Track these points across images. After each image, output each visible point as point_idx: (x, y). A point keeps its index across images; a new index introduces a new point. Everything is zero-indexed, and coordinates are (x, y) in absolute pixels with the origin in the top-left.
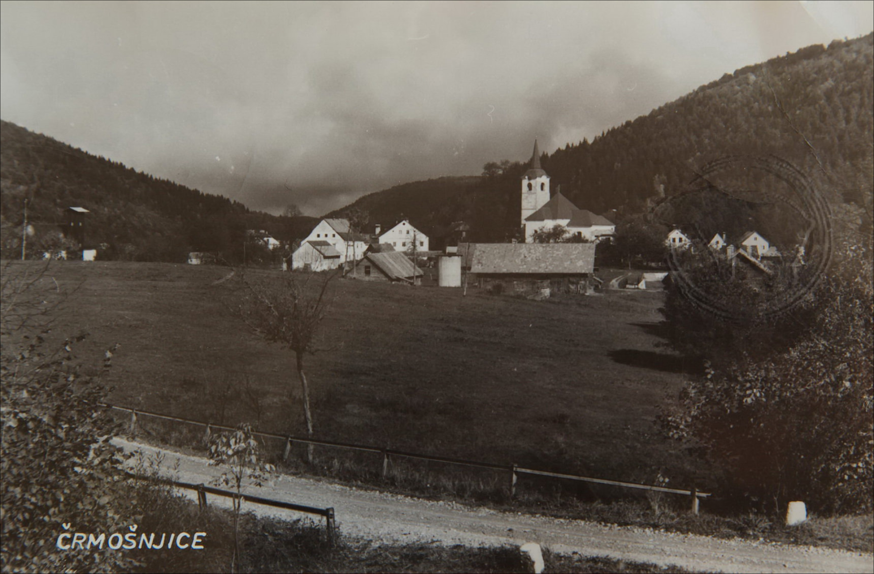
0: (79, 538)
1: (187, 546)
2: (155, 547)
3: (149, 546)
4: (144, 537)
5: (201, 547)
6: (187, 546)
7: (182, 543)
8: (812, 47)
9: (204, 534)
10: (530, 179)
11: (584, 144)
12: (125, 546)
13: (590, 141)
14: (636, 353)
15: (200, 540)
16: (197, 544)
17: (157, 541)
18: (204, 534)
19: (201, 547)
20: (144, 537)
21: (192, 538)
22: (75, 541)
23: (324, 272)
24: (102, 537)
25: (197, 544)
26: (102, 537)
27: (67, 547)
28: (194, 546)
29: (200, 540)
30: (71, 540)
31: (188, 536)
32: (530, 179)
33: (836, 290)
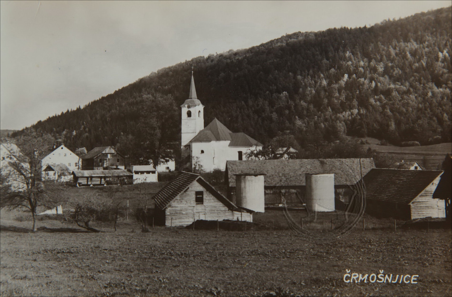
0: (355, 276)
1: (409, 281)
2: (393, 282)
3: (390, 281)
4: (387, 276)
5: (416, 283)
6: (409, 281)
7: (407, 280)
8: (331, 33)
9: (418, 276)
10: (189, 107)
11: (79, 109)
12: (378, 281)
13: (82, 107)
14: (297, 186)
15: (416, 279)
16: (414, 281)
17: (394, 278)
18: (418, 276)
19: (416, 283)
20: (387, 276)
21: (411, 278)
22: (353, 277)
23: (395, 124)
24: (366, 276)
25: (414, 281)
26: (366, 276)
27: (348, 281)
28: (412, 282)
29: (416, 279)
30: (350, 278)
31: (410, 276)
32: (189, 107)
33: (237, 166)
